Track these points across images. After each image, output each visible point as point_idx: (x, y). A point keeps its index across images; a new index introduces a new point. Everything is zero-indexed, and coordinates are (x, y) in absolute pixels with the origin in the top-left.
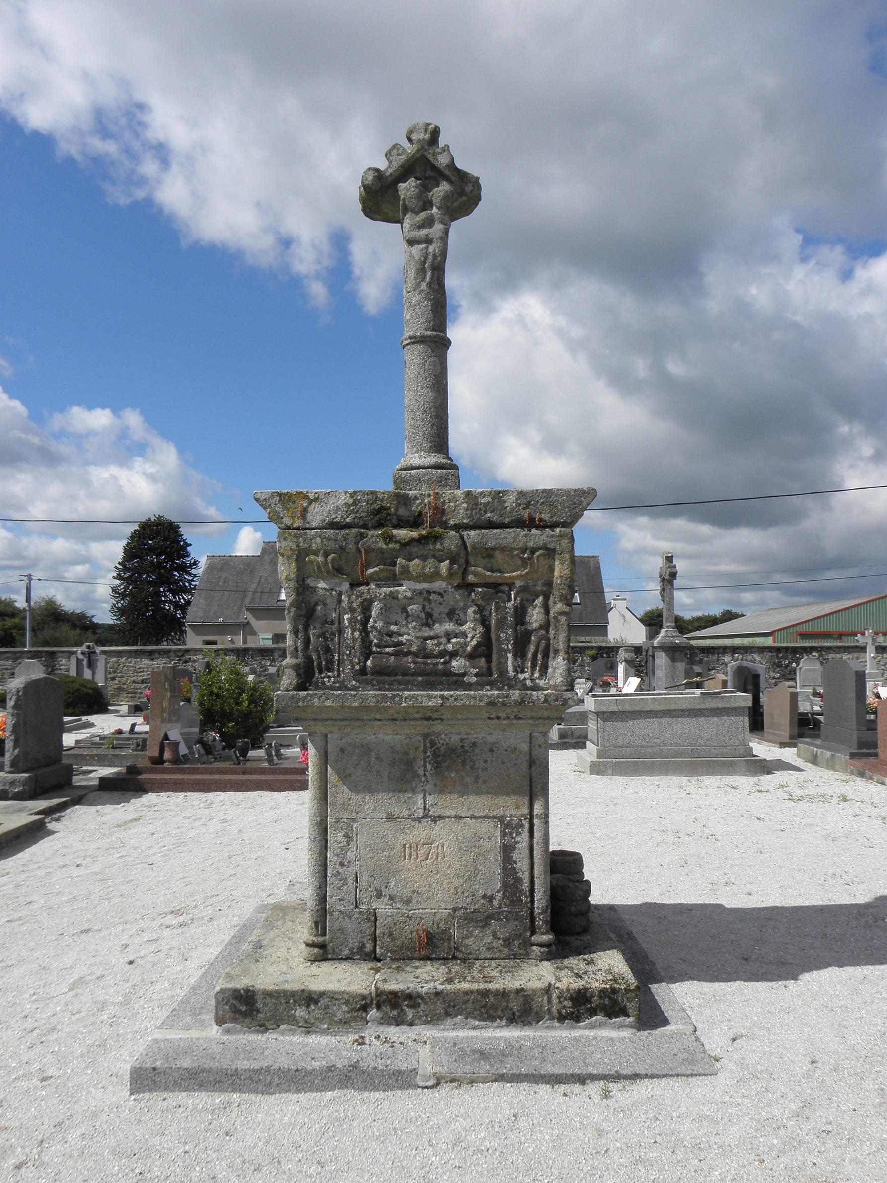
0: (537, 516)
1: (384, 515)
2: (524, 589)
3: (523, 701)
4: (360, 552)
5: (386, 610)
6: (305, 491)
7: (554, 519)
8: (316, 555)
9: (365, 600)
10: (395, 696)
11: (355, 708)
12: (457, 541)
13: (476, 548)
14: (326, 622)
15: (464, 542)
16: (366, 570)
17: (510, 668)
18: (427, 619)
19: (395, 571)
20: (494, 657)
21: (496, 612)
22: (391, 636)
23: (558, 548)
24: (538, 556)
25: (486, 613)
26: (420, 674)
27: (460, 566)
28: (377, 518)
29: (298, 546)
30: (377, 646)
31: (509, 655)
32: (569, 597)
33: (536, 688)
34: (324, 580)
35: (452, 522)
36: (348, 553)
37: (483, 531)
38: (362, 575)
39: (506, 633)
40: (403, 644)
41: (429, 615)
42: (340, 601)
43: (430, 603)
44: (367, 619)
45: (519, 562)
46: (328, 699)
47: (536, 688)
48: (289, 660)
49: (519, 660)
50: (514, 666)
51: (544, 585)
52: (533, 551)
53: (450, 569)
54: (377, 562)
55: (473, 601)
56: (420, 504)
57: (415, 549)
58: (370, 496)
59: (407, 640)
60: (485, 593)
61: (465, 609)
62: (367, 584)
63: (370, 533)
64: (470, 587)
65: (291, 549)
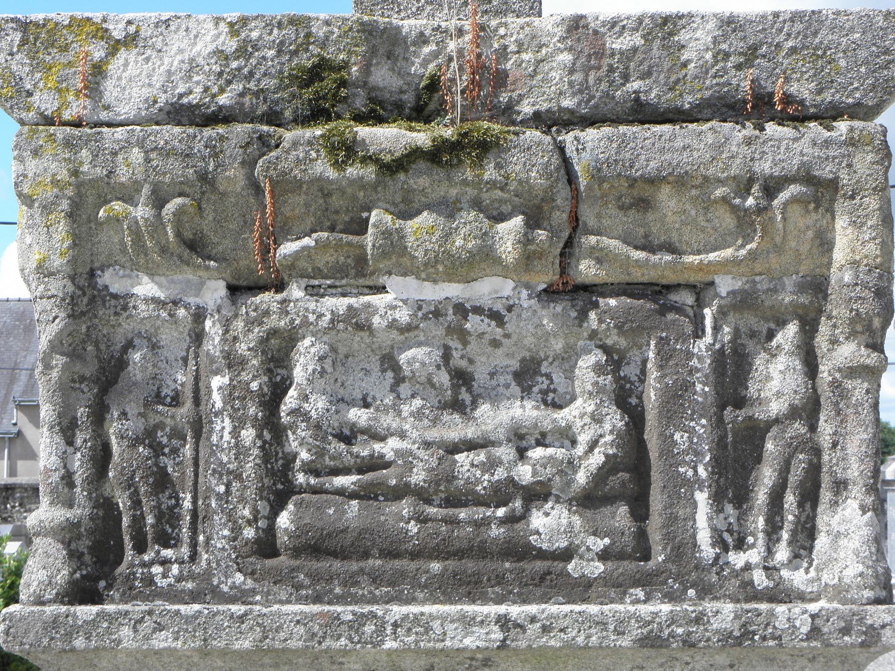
0: (778, 89)
1: (329, 83)
2: (743, 301)
3: (747, 633)
4: (257, 189)
5: (334, 360)
6: (97, 17)
7: (827, 96)
8: (129, 199)
9: (274, 332)
10: (361, 619)
11: (242, 654)
12: (546, 158)
13: (602, 180)
14: (159, 398)
15: (566, 162)
16: (277, 244)
17: (704, 537)
18: (455, 388)
19: (362, 247)
20: (657, 500)
21: (661, 367)
22: (348, 440)
23: (844, 176)
24: (786, 204)
25: (630, 371)
26: (436, 553)
27: (554, 232)
28: (308, 93)
29: (75, 173)
30: (311, 469)
31: (702, 498)
32: (877, 323)
33: (780, 594)
34: (152, 275)
35: (526, 109)
36: (224, 194)
37: (623, 129)
38: (264, 260)
39: (691, 432)
40: (388, 465)
41: (462, 378)
42: (198, 337)
43: (465, 343)
44: (279, 390)
45: (729, 221)
46: (160, 627)
47: (780, 594)
48: (45, 514)
49: (729, 509)
50: (714, 529)
51: (802, 288)
52: (771, 188)
53: (526, 241)
54: (310, 221)
55: (593, 335)
56: (435, 55)
57: (421, 180)
58: (289, 32)
59: (397, 452)
60: (628, 311)
61: (568, 359)
62: (280, 287)
63: (289, 136)
64: (584, 294)
65: (55, 183)
